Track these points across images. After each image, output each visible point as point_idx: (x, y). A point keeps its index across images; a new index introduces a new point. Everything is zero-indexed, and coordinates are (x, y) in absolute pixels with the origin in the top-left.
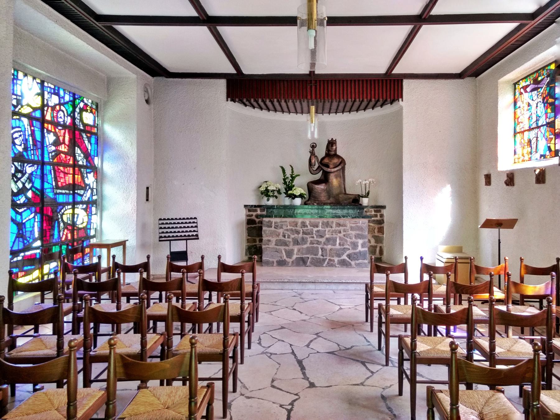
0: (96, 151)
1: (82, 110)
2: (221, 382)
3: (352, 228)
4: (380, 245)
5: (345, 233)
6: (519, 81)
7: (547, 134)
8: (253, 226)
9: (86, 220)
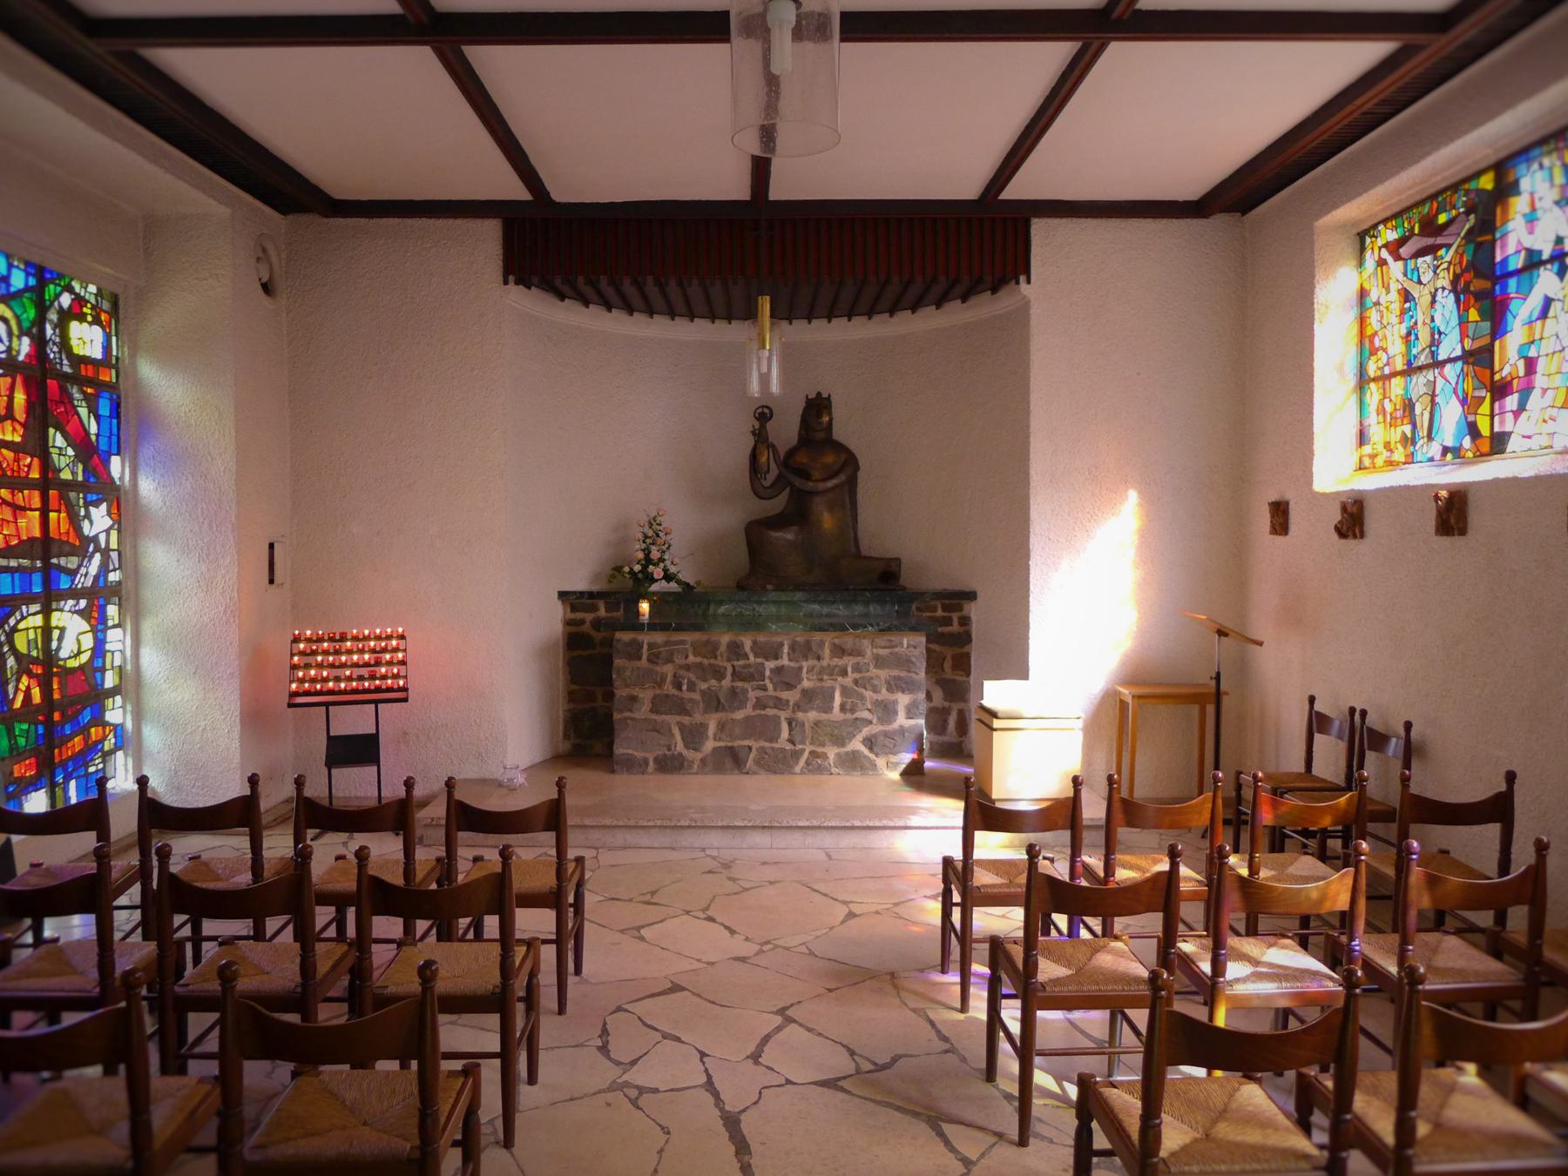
0: (114, 439)
1: (66, 316)
2: (497, 1062)
3: (880, 662)
4: (960, 705)
5: (857, 676)
6: (1375, 226)
7: (1469, 385)
8: (585, 653)
9: (88, 642)
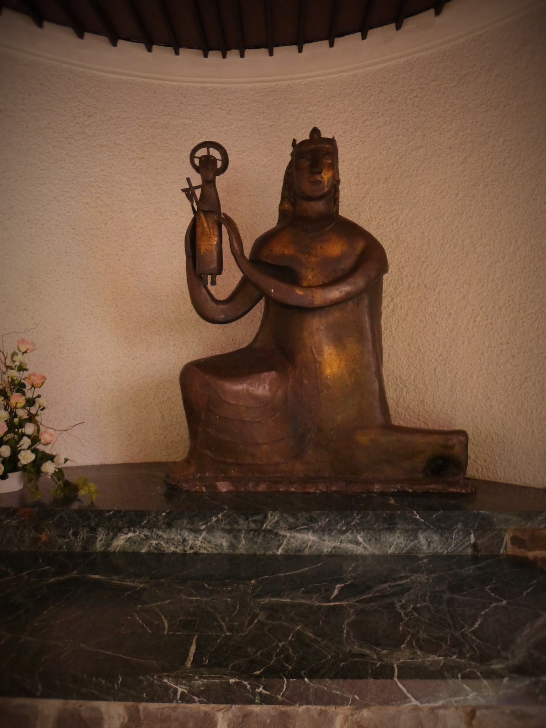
7: (162, 549)
